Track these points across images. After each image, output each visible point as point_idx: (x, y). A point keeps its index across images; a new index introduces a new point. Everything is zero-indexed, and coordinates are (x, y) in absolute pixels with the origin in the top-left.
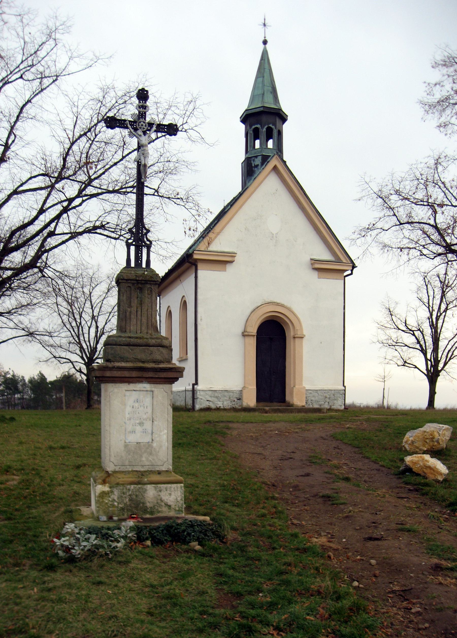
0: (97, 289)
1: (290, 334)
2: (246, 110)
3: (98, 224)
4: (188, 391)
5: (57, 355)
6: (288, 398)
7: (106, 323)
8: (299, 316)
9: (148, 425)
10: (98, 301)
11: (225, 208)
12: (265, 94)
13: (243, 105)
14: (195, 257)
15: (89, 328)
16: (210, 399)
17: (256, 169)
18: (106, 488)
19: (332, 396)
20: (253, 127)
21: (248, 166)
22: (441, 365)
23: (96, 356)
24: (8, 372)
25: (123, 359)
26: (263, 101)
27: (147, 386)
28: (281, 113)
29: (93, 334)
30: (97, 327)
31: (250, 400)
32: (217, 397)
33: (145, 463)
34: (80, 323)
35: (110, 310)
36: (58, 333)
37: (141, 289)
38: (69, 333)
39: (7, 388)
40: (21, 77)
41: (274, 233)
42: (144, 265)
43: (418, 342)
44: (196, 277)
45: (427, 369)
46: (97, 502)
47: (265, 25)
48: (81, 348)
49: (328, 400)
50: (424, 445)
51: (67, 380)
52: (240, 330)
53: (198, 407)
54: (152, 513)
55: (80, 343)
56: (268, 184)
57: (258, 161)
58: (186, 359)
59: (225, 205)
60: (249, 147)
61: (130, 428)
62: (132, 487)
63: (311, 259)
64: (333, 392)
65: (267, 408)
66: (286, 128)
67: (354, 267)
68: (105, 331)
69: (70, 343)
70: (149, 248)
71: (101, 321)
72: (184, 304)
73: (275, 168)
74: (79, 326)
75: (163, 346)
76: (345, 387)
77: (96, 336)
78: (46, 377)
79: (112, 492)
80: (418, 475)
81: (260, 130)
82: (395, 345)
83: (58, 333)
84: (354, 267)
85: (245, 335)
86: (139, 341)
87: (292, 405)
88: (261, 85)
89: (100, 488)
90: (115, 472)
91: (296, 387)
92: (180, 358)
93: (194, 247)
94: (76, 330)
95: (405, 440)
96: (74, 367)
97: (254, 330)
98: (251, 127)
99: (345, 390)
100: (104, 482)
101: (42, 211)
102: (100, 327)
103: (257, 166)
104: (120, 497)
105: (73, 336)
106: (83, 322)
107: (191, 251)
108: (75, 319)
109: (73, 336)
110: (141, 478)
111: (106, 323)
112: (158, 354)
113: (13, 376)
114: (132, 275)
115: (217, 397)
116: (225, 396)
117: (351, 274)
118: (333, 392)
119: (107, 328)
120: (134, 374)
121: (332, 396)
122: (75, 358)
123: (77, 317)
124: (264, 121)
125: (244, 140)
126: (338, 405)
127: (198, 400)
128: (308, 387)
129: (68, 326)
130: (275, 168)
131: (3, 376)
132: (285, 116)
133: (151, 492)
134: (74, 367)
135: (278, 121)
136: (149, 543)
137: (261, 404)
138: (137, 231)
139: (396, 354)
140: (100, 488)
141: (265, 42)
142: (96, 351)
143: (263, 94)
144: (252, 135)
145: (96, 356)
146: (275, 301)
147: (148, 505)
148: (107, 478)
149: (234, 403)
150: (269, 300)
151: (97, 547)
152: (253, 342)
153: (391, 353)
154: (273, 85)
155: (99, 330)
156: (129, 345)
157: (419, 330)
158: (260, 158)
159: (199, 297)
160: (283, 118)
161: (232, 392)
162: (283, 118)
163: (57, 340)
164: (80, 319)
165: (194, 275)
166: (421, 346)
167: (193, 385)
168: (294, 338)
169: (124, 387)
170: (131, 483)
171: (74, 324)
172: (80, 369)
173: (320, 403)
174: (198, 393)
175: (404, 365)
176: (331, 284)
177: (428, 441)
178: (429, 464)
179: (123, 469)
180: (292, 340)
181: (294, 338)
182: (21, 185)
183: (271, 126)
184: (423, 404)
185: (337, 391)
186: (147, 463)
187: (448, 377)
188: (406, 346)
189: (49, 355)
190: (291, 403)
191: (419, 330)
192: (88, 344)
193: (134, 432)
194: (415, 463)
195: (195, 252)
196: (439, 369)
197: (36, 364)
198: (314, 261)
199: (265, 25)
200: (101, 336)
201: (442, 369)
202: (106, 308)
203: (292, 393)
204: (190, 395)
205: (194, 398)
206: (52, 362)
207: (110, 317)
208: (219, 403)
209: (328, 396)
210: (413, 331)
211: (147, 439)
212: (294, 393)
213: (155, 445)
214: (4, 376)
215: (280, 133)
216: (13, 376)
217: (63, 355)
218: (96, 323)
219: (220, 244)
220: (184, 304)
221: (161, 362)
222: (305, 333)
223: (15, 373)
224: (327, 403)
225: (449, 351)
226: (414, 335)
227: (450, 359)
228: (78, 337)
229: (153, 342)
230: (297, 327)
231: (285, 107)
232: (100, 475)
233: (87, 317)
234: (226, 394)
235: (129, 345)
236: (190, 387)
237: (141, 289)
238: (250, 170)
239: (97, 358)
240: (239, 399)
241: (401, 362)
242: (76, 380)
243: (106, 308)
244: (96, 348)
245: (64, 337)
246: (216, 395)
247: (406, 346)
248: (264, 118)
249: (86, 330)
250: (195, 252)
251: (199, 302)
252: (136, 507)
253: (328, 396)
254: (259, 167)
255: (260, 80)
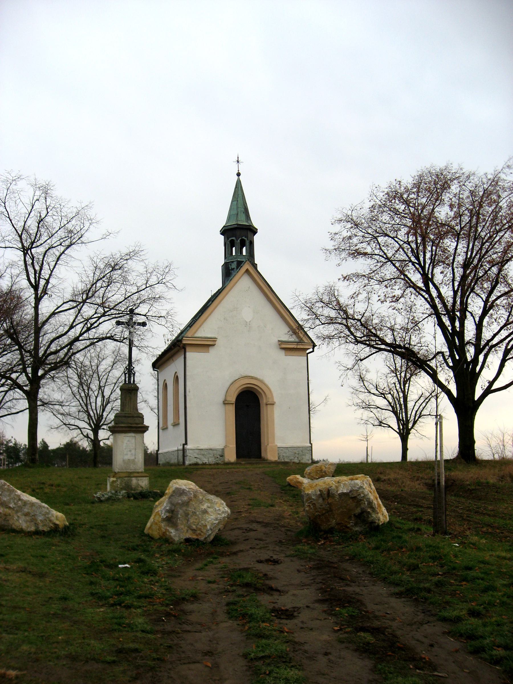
0: (104, 362)
1: (263, 401)
2: (224, 227)
3: (108, 335)
4: (180, 450)
5: (67, 423)
6: (263, 455)
7: (111, 393)
8: (270, 386)
9: (133, 452)
10: (104, 374)
11: (212, 297)
12: (239, 214)
13: (222, 221)
14: (184, 342)
15: (96, 397)
16: (197, 456)
17: (232, 271)
18: (115, 479)
19: (301, 452)
20: (230, 239)
21: (226, 269)
22: (410, 425)
23: (102, 423)
24: (10, 440)
25: (122, 423)
26: (237, 220)
27: (133, 434)
28: (251, 228)
29: (99, 403)
30: (103, 397)
31: (231, 456)
32: (203, 455)
33: (132, 468)
34: (88, 394)
35: (115, 381)
36: (69, 403)
37: (131, 393)
38: (78, 402)
39: (9, 457)
40: (61, 245)
41: (248, 321)
42: (132, 382)
43: (390, 403)
44: (185, 358)
45: (399, 428)
46: (111, 485)
47: (238, 162)
48: (89, 415)
49: (297, 456)
50: (316, 475)
51: (71, 447)
52: (221, 398)
53: (187, 463)
54: (134, 490)
55: (87, 411)
56: (243, 284)
57: (234, 265)
58: (179, 424)
59: (213, 294)
60: (228, 253)
61: (125, 453)
62: (126, 478)
63: (279, 341)
64: (301, 449)
65: (243, 462)
66: (257, 238)
67: (314, 346)
68: (110, 400)
69: (79, 411)
70: (134, 374)
71: (107, 392)
72: (176, 379)
73: (247, 271)
74: (87, 396)
75: (140, 417)
76: (312, 444)
77: (103, 404)
78: (49, 445)
79: (117, 481)
80: (293, 487)
81: (235, 241)
82: (368, 407)
83: (69, 403)
84: (314, 346)
85: (225, 403)
86: (129, 415)
87: (267, 460)
88: (235, 207)
89: (112, 479)
90: (119, 472)
91: (270, 445)
92: (174, 423)
93: (183, 335)
94: (84, 399)
95: (305, 472)
96: (82, 433)
97: (233, 399)
98: (228, 239)
99: (312, 447)
100: (114, 477)
101: (72, 327)
102: (106, 397)
103: (233, 269)
104: (121, 483)
105: (82, 406)
106: (91, 393)
107: (180, 338)
108: (84, 390)
109: (82, 406)
110: (130, 475)
111: (111, 393)
112: (137, 420)
113: (15, 444)
114: (126, 387)
115: (203, 455)
116: (209, 454)
117: (313, 351)
118: (301, 449)
119: (113, 397)
120: (127, 429)
121: (301, 452)
122: (82, 424)
123: (85, 388)
124: (239, 234)
125: (224, 248)
126: (306, 459)
127: (188, 458)
128: (279, 445)
129: (78, 397)
130: (247, 271)
131: (5, 445)
132: (255, 230)
133: (134, 481)
134: (82, 433)
135: (249, 234)
136: (132, 499)
137: (240, 460)
138: (129, 367)
139: (372, 415)
140: (112, 479)
141: (239, 174)
142: (102, 418)
143: (237, 214)
144: (229, 245)
145: (102, 423)
146: (250, 375)
147: (133, 487)
148: (115, 474)
149: (217, 459)
150: (245, 375)
151: (111, 496)
152: (232, 409)
153: (366, 414)
154: (245, 207)
155: (105, 400)
156: (125, 417)
157: (390, 393)
158: (235, 263)
159: (188, 373)
160: (254, 231)
161: (216, 450)
162: (254, 231)
163: (66, 409)
164: (88, 390)
165: (183, 356)
166: (392, 407)
167: (184, 445)
168: (267, 404)
169: (123, 435)
170: (126, 477)
171: (83, 394)
172: (87, 435)
173: (291, 458)
174: (188, 452)
175: (380, 425)
176: (295, 361)
177: (318, 472)
178: (299, 480)
179: (122, 471)
180: (265, 406)
181: (267, 404)
182: (57, 309)
183: (244, 238)
184: (398, 458)
185: (304, 448)
186: (132, 468)
187: (417, 435)
188: (378, 407)
189: (58, 422)
190: (266, 458)
191: (390, 393)
192: (95, 412)
193: (127, 454)
194: (292, 480)
195: (184, 338)
196: (410, 428)
197: (49, 430)
198: (281, 342)
199: (238, 162)
200: (107, 405)
201: (412, 427)
202: (112, 379)
203: (266, 450)
204: (181, 453)
205: (184, 456)
206: (62, 429)
207: (115, 387)
208: (205, 459)
209: (297, 453)
210: (383, 394)
211: (133, 458)
212: (268, 450)
213: (136, 460)
214: (6, 445)
215: (252, 243)
216: (15, 444)
217: (72, 422)
218: (103, 393)
219: (205, 331)
220: (176, 379)
221: (139, 424)
222: (276, 400)
223: (18, 442)
224: (296, 458)
225: (417, 411)
226: (385, 398)
227: (419, 417)
228: (86, 405)
229: (135, 415)
230: (269, 396)
231: (255, 223)
232: (112, 474)
233: (94, 386)
234: (211, 452)
235: (125, 417)
236: (181, 447)
237: (131, 393)
238: (228, 272)
239: (103, 425)
240: (222, 456)
241: (377, 423)
242: (79, 448)
243: (112, 379)
244: (102, 415)
245: (73, 407)
246: (202, 452)
247: (378, 407)
248: (238, 233)
249: (93, 400)
250: (184, 338)
251: (187, 377)
252: (128, 487)
253: (297, 453)
254: (235, 270)
255: (235, 203)
